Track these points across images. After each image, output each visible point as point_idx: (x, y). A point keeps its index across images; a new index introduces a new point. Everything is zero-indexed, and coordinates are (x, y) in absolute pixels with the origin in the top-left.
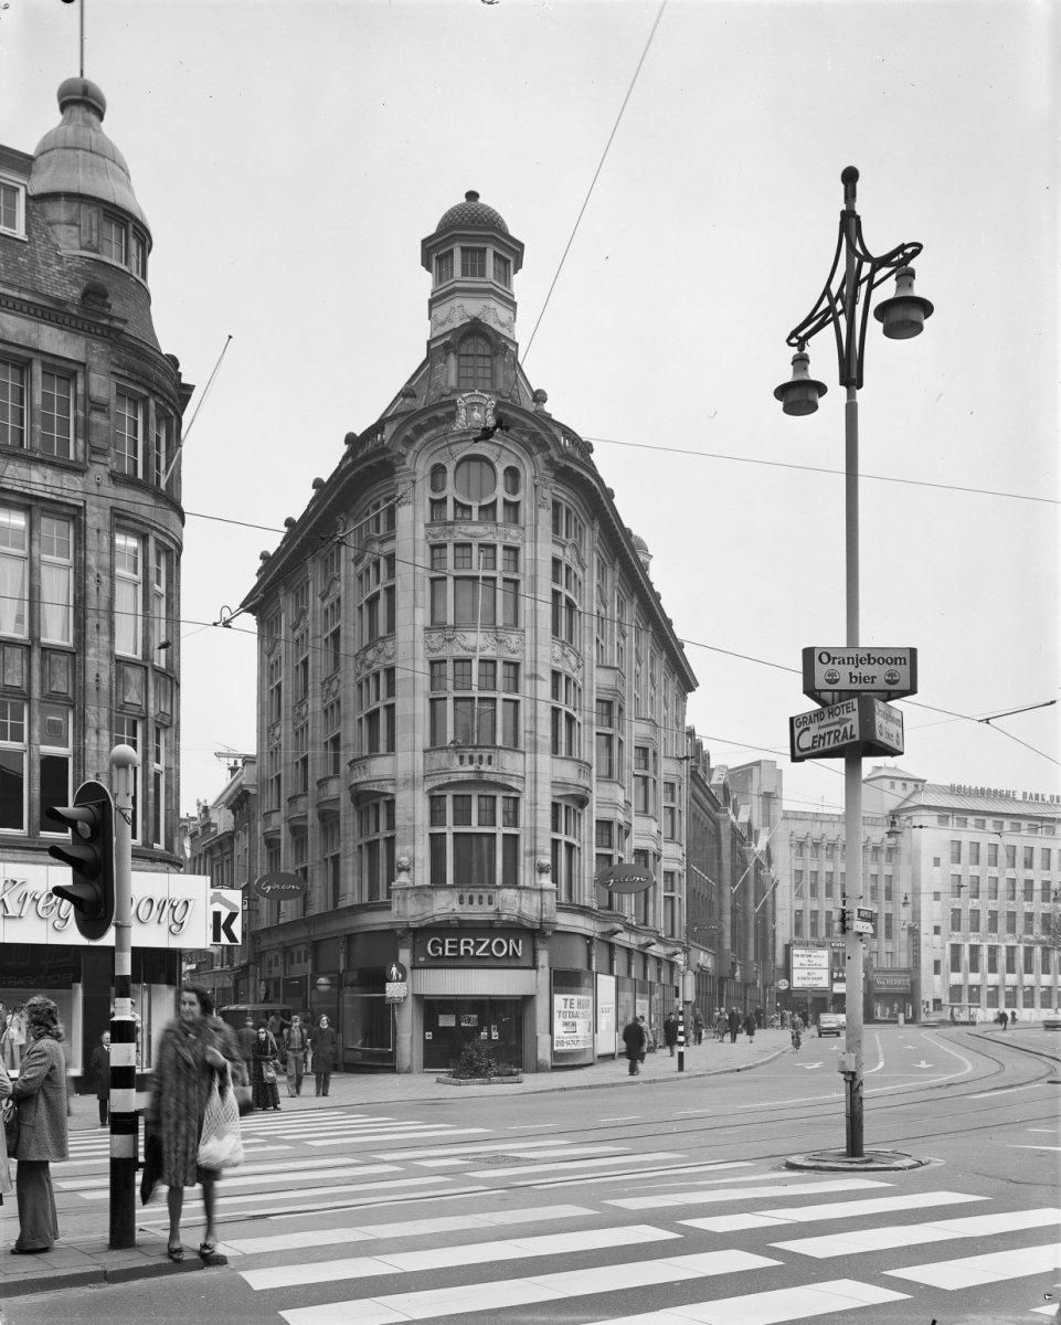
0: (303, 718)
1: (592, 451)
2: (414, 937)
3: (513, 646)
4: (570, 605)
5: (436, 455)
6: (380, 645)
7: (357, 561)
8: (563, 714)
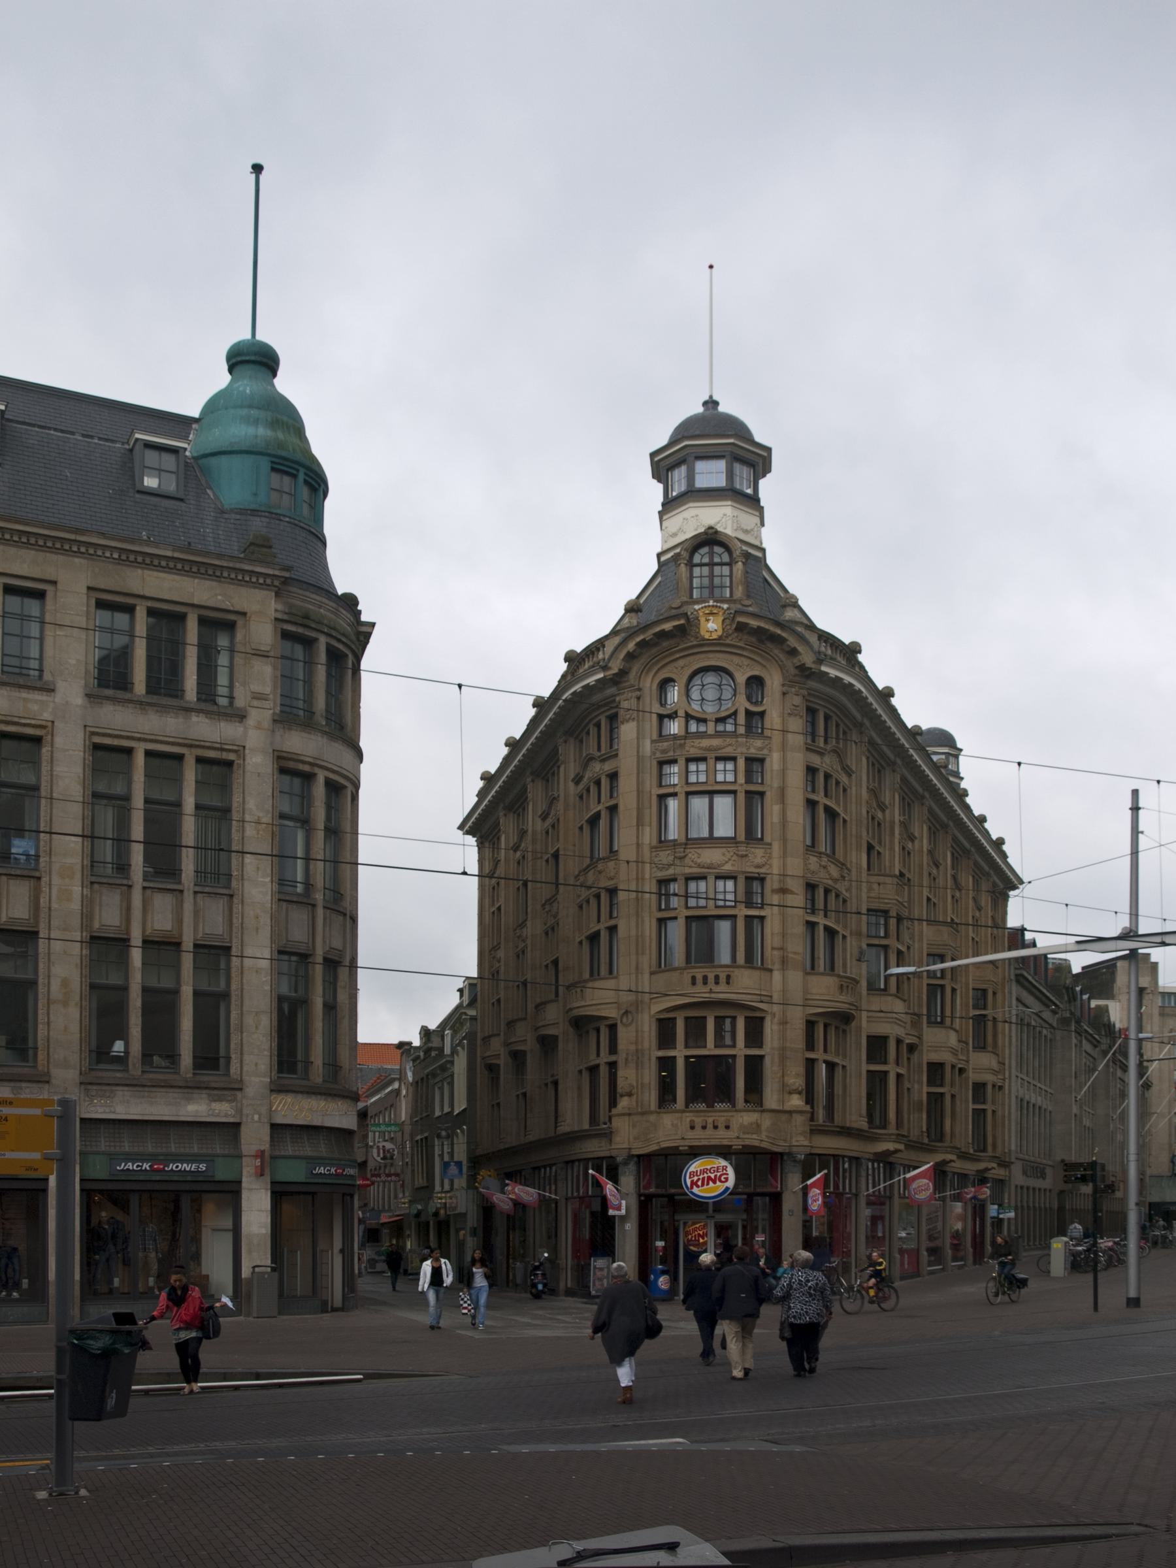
0: (524, 941)
1: (860, 652)
2: (638, 1163)
3: (759, 860)
4: (831, 814)
5: (665, 670)
6: (600, 866)
7: (578, 780)
8: (821, 928)
